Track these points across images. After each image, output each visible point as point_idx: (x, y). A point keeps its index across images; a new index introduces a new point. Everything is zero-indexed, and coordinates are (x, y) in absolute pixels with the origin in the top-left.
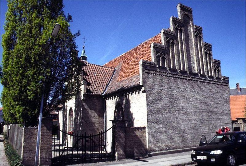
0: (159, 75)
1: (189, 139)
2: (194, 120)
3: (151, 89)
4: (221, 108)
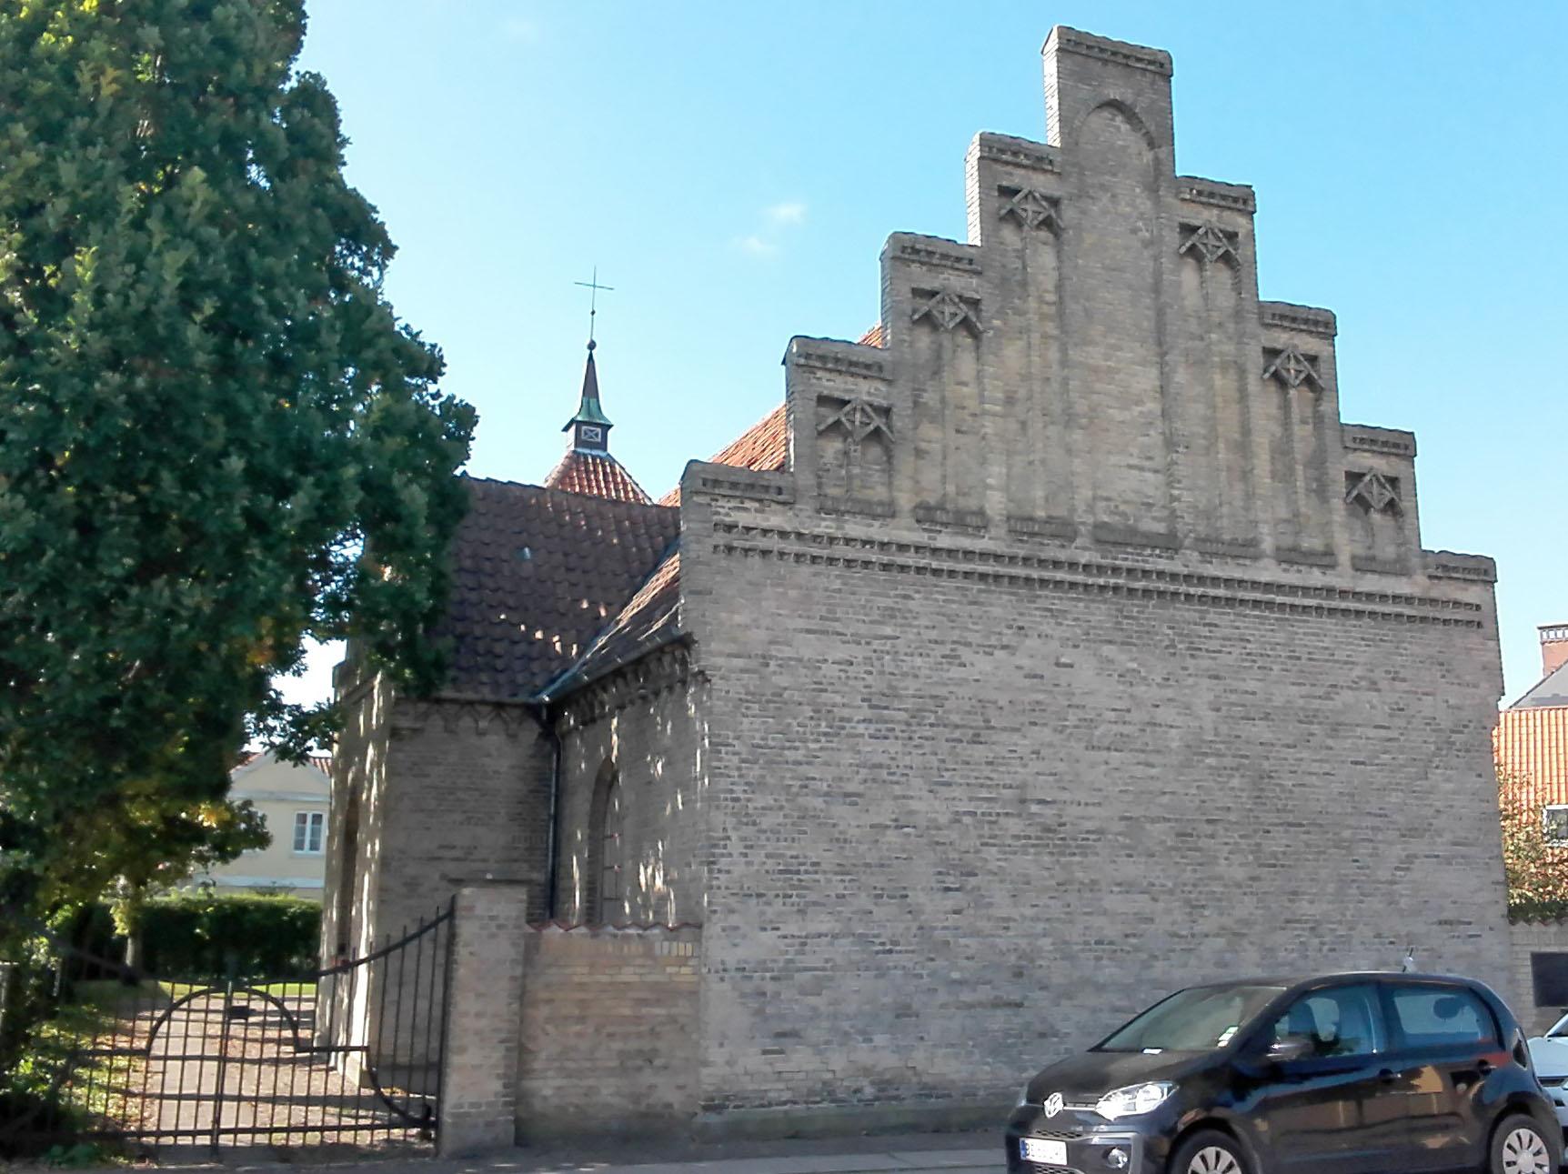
0: (831, 561)
1: (1064, 1028)
2: (1127, 887)
3: (753, 664)
4: (1395, 798)
